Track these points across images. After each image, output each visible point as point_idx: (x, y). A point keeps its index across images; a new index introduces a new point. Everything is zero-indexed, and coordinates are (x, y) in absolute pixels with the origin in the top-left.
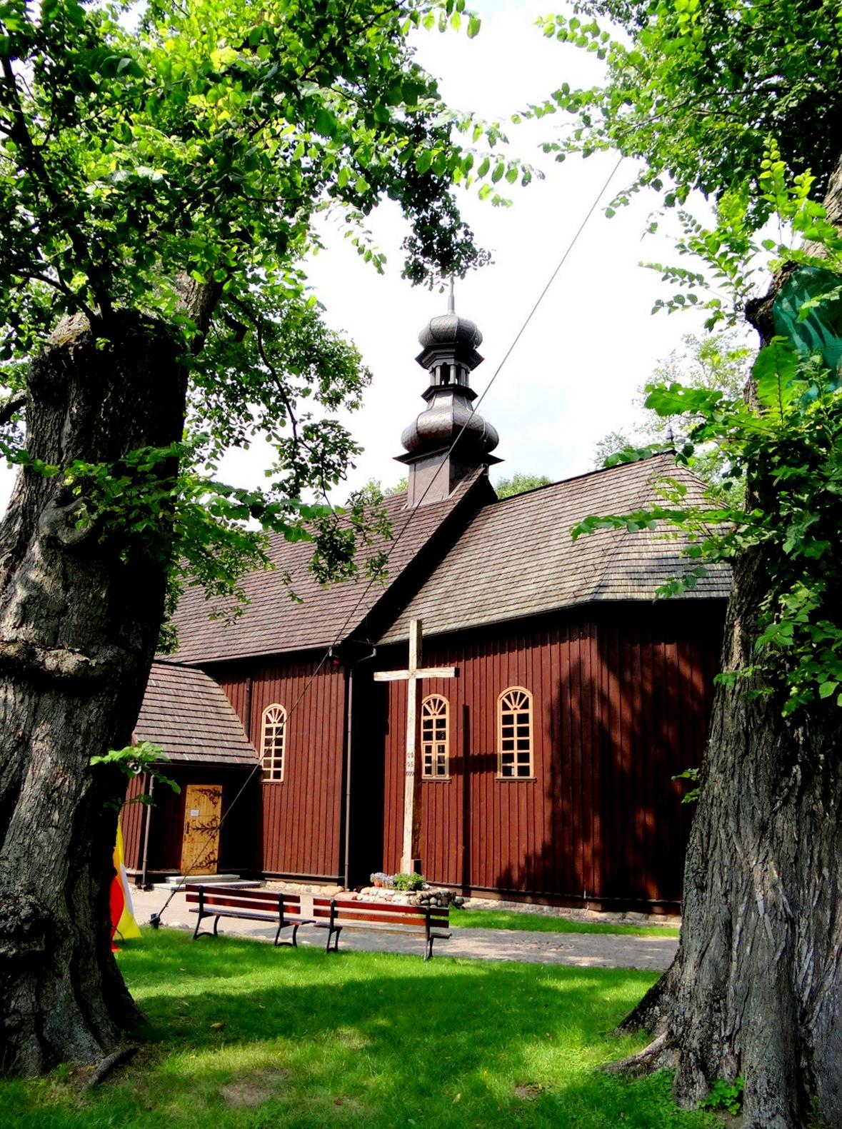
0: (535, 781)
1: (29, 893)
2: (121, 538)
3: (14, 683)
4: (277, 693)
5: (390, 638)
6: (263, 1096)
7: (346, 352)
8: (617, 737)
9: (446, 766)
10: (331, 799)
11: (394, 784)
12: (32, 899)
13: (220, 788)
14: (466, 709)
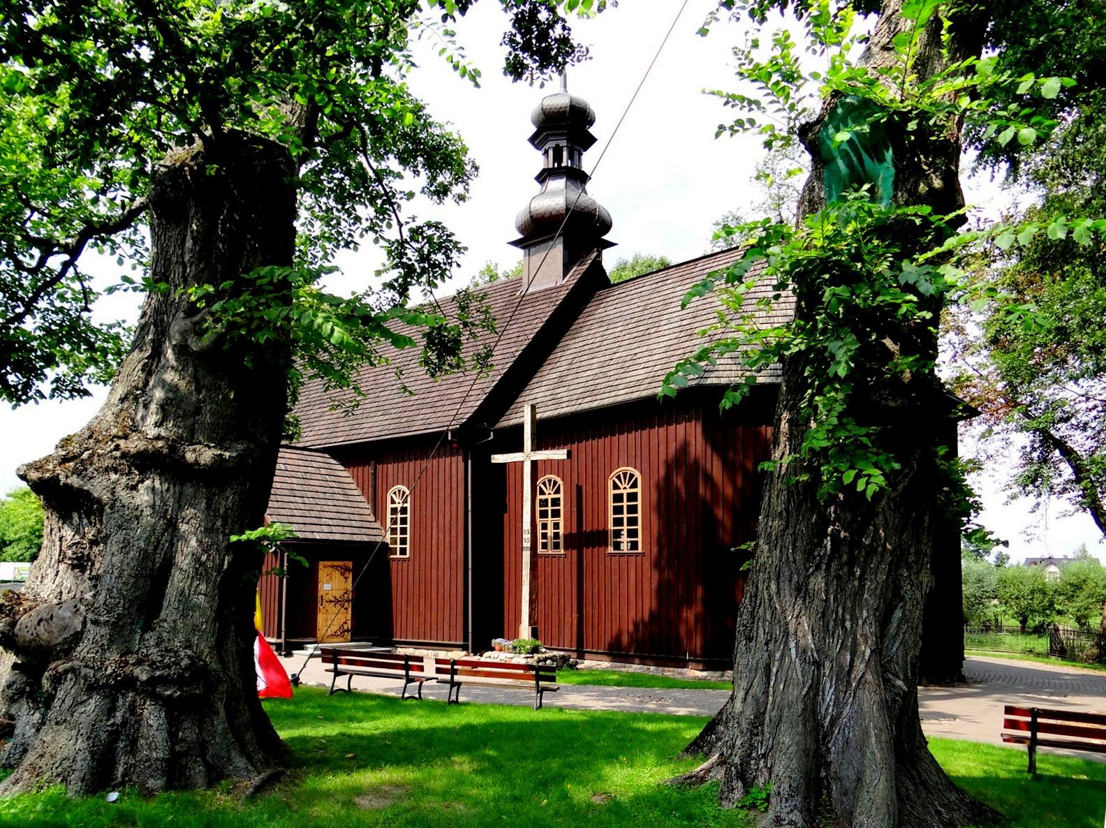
0: (643, 554)
1: (186, 648)
2: (245, 345)
3: (160, 475)
4: (400, 475)
5: (506, 422)
6: (388, 803)
7: (453, 145)
8: (720, 513)
9: (561, 541)
10: (454, 572)
11: (513, 558)
12: (189, 652)
13: (350, 564)
14: (579, 489)
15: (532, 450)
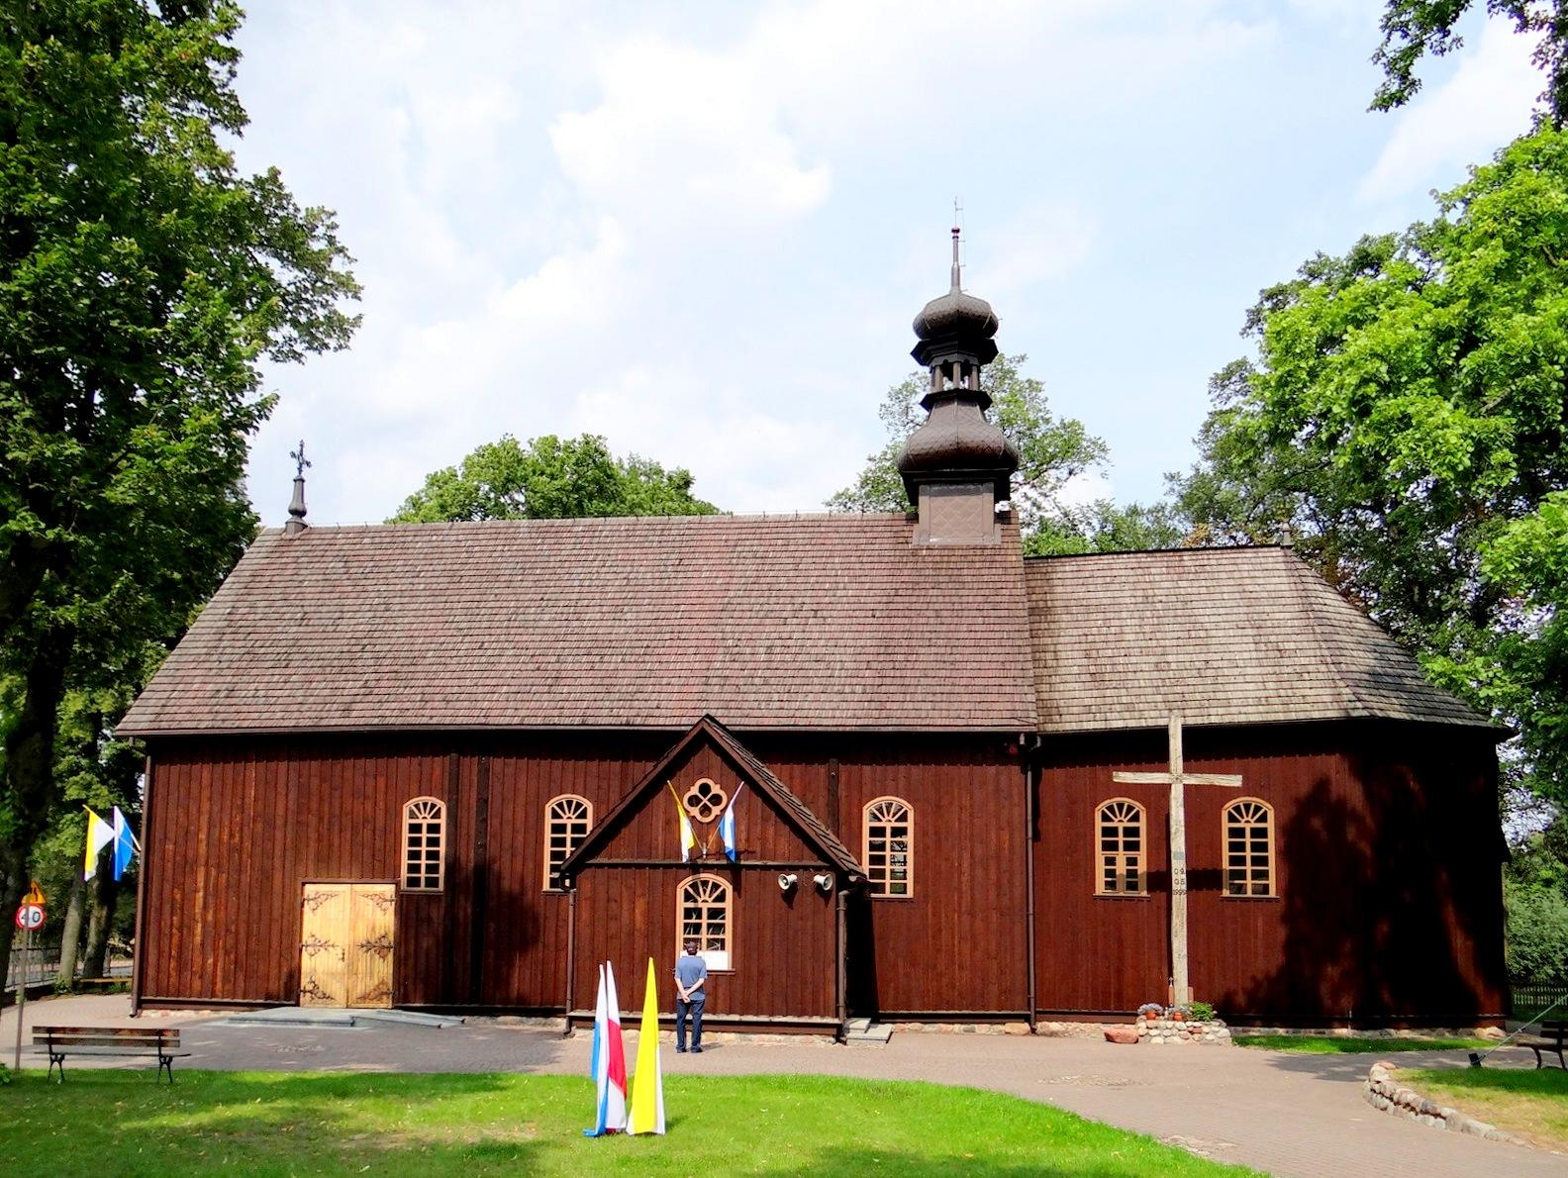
15: (1167, 770)
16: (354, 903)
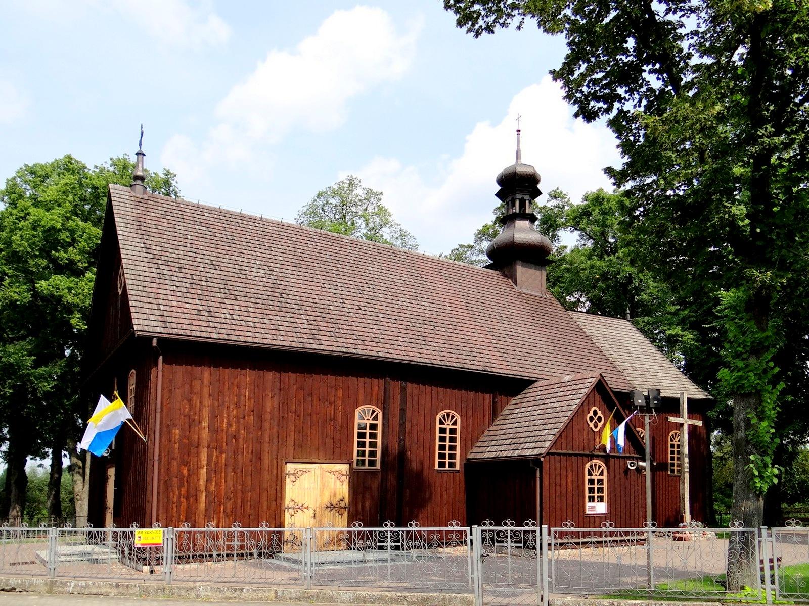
16: (322, 474)
